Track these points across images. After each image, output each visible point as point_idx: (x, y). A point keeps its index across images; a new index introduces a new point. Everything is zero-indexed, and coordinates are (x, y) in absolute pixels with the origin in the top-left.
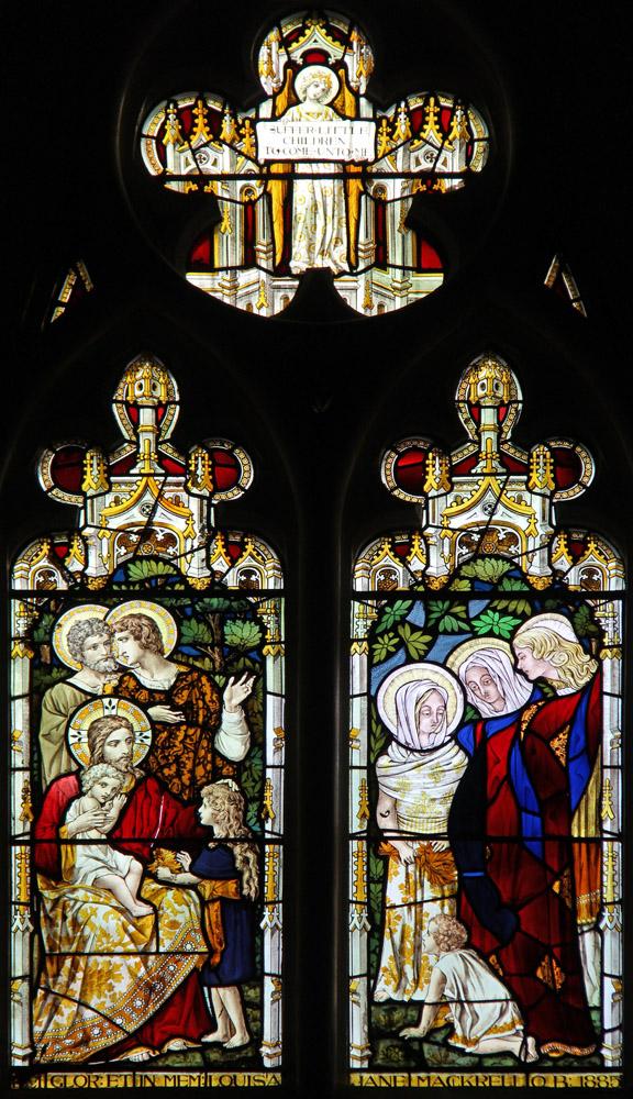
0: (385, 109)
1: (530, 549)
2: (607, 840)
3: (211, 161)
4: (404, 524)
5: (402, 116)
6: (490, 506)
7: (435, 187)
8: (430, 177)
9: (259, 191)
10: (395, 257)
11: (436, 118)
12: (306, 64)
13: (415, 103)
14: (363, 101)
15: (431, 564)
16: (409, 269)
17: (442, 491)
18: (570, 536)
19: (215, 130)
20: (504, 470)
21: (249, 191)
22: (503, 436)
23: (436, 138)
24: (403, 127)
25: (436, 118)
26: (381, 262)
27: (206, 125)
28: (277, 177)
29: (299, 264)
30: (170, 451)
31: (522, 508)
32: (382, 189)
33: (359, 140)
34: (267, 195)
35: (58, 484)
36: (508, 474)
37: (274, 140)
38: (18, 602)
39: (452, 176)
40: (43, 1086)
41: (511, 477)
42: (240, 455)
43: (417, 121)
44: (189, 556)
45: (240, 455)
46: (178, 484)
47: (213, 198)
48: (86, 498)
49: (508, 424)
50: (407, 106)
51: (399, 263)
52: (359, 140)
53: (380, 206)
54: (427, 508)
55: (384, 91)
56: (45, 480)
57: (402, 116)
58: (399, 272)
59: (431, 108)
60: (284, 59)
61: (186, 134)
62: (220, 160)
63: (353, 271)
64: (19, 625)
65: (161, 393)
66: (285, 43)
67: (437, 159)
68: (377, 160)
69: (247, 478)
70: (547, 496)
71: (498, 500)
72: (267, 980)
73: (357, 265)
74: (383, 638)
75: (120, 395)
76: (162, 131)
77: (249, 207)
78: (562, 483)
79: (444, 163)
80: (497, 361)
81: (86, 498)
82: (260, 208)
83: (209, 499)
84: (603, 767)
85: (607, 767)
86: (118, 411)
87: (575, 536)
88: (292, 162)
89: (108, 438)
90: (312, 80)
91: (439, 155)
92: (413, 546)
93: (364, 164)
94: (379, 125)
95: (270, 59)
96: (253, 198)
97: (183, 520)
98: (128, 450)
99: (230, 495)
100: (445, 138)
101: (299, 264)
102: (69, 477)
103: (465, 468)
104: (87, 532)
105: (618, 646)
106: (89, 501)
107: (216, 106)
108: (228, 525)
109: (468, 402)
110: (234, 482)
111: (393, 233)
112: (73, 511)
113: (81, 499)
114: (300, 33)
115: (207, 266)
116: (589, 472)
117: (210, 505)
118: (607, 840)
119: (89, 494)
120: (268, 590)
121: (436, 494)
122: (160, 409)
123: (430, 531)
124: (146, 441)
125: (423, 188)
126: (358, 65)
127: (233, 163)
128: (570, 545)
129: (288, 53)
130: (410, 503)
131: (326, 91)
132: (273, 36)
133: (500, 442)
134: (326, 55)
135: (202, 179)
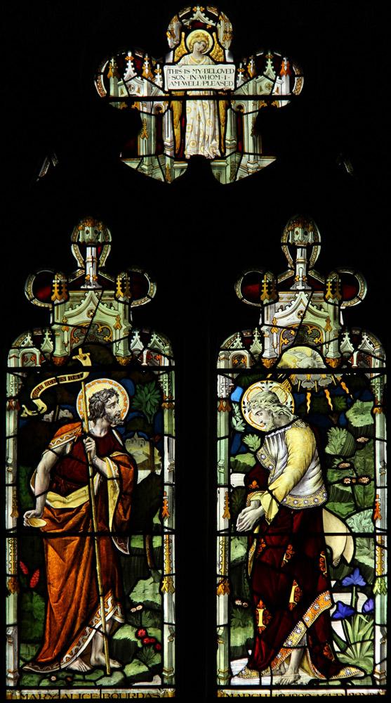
1: (118, 339)
2: (379, 534)
3: (136, 89)
4: (40, 322)
6: (302, 312)
7: (273, 104)
8: (270, 98)
15: (265, 348)
16: (257, 154)
17: (63, 300)
18: (33, 334)
20: (101, 287)
21: (159, 108)
22: (100, 266)
23: (272, 75)
28: (177, 98)
29: (190, 151)
30: (313, 274)
31: (322, 312)
32: (240, 107)
34: (170, 108)
36: (103, 290)
38: (11, 375)
39: (282, 98)
41: (105, 292)
44: (117, 343)
46: (111, 296)
47: (138, 112)
48: (54, 306)
52: (225, 77)
53: (239, 116)
54: (53, 312)
56: (29, 290)
58: (252, 157)
62: (141, 88)
63: (223, 157)
64: (12, 390)
65: (310, 238)
67: (273, 88)
68: (236, 88)
70: (337, 305)
71: (97, 307)
72: (166, 627)
73: (225, 152)
74: (157, 399)
75: (284, 240)
76: (107, 70)
77: (159, 117)
79: (277, 91)
81: (54, 306)
83: (130, 305)
84: (376, 487)
86: (286, 249)
88: (186, 90)
89: (69, 266)
91: (274, 85)
93: (229, 91)
97: (113, 316)
98: (290, 273)
99: (352, 302)
100: (276, 75)
101: (190, 151)
102: (43, 289)
104: (264, 328)
106: (56, 307)
108: (140, 321)
110: (354, 295)
112: (47, 313)
113: (51, 306)
116: (153, 290)
118: (379, 534)
119: (55, 303)
120: (164, 367)
121: (59, 302)
122: (309, 248)
123: (55, 327)
124: (300, 269)
125: (266, 105)
127: (150, 89)
130: (44, 308)
135: (131, 99)
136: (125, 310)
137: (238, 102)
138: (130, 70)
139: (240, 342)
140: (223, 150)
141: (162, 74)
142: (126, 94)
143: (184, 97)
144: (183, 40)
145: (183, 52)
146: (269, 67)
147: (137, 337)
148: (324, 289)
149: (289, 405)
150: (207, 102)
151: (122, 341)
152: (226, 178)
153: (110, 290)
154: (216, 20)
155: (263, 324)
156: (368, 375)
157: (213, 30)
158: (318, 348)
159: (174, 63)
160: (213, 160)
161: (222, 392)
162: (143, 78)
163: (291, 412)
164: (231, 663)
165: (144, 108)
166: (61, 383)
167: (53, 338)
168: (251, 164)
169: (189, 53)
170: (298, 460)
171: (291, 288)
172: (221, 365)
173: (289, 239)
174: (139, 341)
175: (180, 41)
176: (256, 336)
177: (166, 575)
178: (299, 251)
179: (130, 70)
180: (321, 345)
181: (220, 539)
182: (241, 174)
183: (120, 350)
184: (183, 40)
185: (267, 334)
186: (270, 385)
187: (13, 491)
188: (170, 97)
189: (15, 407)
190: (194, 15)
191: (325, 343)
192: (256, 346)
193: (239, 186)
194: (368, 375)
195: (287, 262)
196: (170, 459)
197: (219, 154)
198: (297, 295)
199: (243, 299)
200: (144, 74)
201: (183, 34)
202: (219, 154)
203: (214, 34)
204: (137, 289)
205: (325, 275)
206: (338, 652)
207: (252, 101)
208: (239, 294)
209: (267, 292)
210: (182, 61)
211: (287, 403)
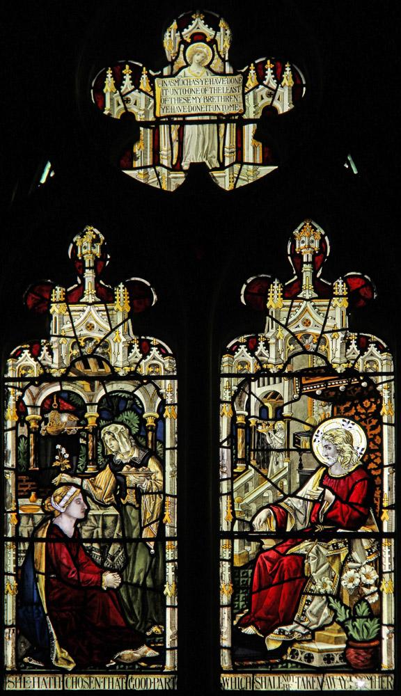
10: (248, 156)
11: (272, 71)
12: (193, 42)
23: (273, 85)
25: (272, 71)
26: (240, 160)
55: (239, 59)
60: (179, 39)
95: (170, 40)
129: (181, 36)
138: (127, 84)
144: (181, 53)
149: (359, 451)
150: (196, 126)
159: (172, 75)
162: (141, 91)
163: (230, 389)
164: (224, 669)
166: (46, 612)
167: (267, 346)
168: (248, 176)
169: (188, 65)
171: (81, 301)
172: (225, 370)
175: (178, 53)
177: (95, 404)
179: (127, 84)
182: (240, 184)
184: (181, 53)
186: (351, 425)
189: (84, 255)
196: (172, 464)
198: (301, 304)
200: (141, 87)
201: (182, 46)
203: (214, 46)
206: (297, 627)
208: (155, 297)
210: (181, 73)
211: (358, 448)
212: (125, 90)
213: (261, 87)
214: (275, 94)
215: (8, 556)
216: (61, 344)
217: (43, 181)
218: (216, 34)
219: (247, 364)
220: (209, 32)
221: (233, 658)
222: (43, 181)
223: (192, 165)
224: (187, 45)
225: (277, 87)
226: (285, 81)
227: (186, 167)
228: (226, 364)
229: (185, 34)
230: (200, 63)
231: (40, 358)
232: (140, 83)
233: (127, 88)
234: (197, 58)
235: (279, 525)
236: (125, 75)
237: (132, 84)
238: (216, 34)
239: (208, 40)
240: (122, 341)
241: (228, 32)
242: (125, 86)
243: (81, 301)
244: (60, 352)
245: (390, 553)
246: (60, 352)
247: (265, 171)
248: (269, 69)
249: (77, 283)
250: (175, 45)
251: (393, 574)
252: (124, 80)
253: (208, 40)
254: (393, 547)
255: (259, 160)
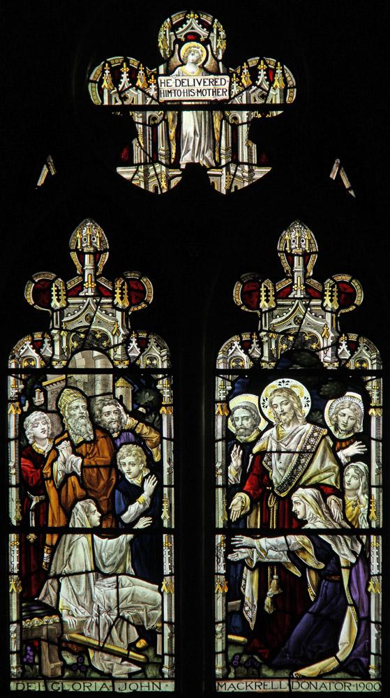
0: (235, 67)
5: (245, 71)
9: (160, 118)
10: (243, 155)
11: (265, 73)
12: (187, 40)
13: (253, 62)
14: (220, 63)
19: (133, 80)
22: (308, 275)
23: (266, 86)
24: (246, 81)
25: (265, 73)
26: (235, 159)
27: (127, 77)
29: (185, 159)
33: (220, 88)
35: (349, 284)
37: (172, 86)
40: (106, 103)
42: (31, 302)
43: (254, 73)
45: (31, 302)
49: (310, 267)
50: (247, 64)
51: (246, 160)
52: (220, 88)
55: (232, 61)
56: (238, 300)
57: (245, 71)
59: (262, 66)
60: (173, 38)
61: (116, 80)
66: (174, 28)
68: (230, 99)
69: (359, 299)
75: (280, 247)
78: (343, 305)
80: (302, 225)
82: (160, 129)
85: (374, 486)
86: (74, 256)
87: (143, 305)
88: (181, 101)
90: (193, 51)
92: (253, 343)
94: (231, 77)
95: (165, 38)
96: (156, 122)
97: (111, 324)
100: (271, 85)
101: (185, 159)
103: (75, 292)
105: (380, 407)
106: (55, 313)
107: (134, 62)
109: (285, 252)
111: (242, 147)
113: (259, 313)
114: (184, 21)
115: (129, 162)
116: (359, 299)
117: (127, 314)
126: (219, 45)
127: (144, 99)
128: (349, 343)
129: (175, 35)
131: (199, 59)
132: (167, 23)
133: (305, 278)
134: (199, 36)
135: (128, 109)
136: (332, 318)
137: (234, 113)
139: (30, 344)
140: (217, 158)
141: (157, 84)
142: (120, 103)
143: (179, 107)
145: (178, 64)
146: (262, 76)
147: (134, 344)
148: (112, 295)
151: (120, 347)
152: (222, 186)
153: (107, 297)
154: (210, 29)
155: (262, 330)
156: (154, 376)
157: (206, 42)
158: (105, 352)
160: (208, 169)
161: (220, 395)
162: (138, 88)
165: (137, 117)
167: (261, 345)
169: (183, 64)
170: (233, 459)
171: (290, 296)
172: (220, 366)
173: (286, 246)
174: (346, 350)
176: (254, 341)
178: (87, 257)
180: (108, 348)
181: (219, 538)
183: (326, 357)
185: (265, 339)
187: (223, 492)
188: (165, 107)
190: (188, 21)
191: (323, 349)
192: (47, 351)
193: (235, 196)
194: (154, 376)
195: (76, 269)
197: (214, 164)
199: (34, 305)
201: (177, 46)
202: (214, 164)
203: (209, 46)
204: (136, 294)
205: (112, 280)
207: (246, 112)
209: (265, 300)
212: (123, 88)
213: (254, 88)
214: (268, 95)
215: (12, 552)
216: (271, 339)
217: (41, 182)
218: (209, 34)
219: (242, 361)
220: (203, 33)
221: (21, 663)
222: (41, 182)
223: (188, 164)
224: (181, 44)
225: (270, 89)
226: (276, 83)
227: (183, 167)
228: (221, 361)
229: (180, 33)
230: (195, 63)
231: (250, 351)
232: (137, 80)
233: (124, 86)
234: (191, 58)
235: (264, 521)
236: (260, 70)
237: (129, 82)
238: (209, 34)
239: (202, 39)
240: (331, 336)
241: (222, 33)
242: (122, 84)
243: (290, 296)
244: (270, 346)
245: (378, 553)
246: (270, 346)
247: (260, 173)
248: (125, 73)
249: (313, 277)
250: (170, 44)
251: (381, 577)
252: (122, 78)
253: (202, 39)
254: (381, 547)
255: (255, 161)
